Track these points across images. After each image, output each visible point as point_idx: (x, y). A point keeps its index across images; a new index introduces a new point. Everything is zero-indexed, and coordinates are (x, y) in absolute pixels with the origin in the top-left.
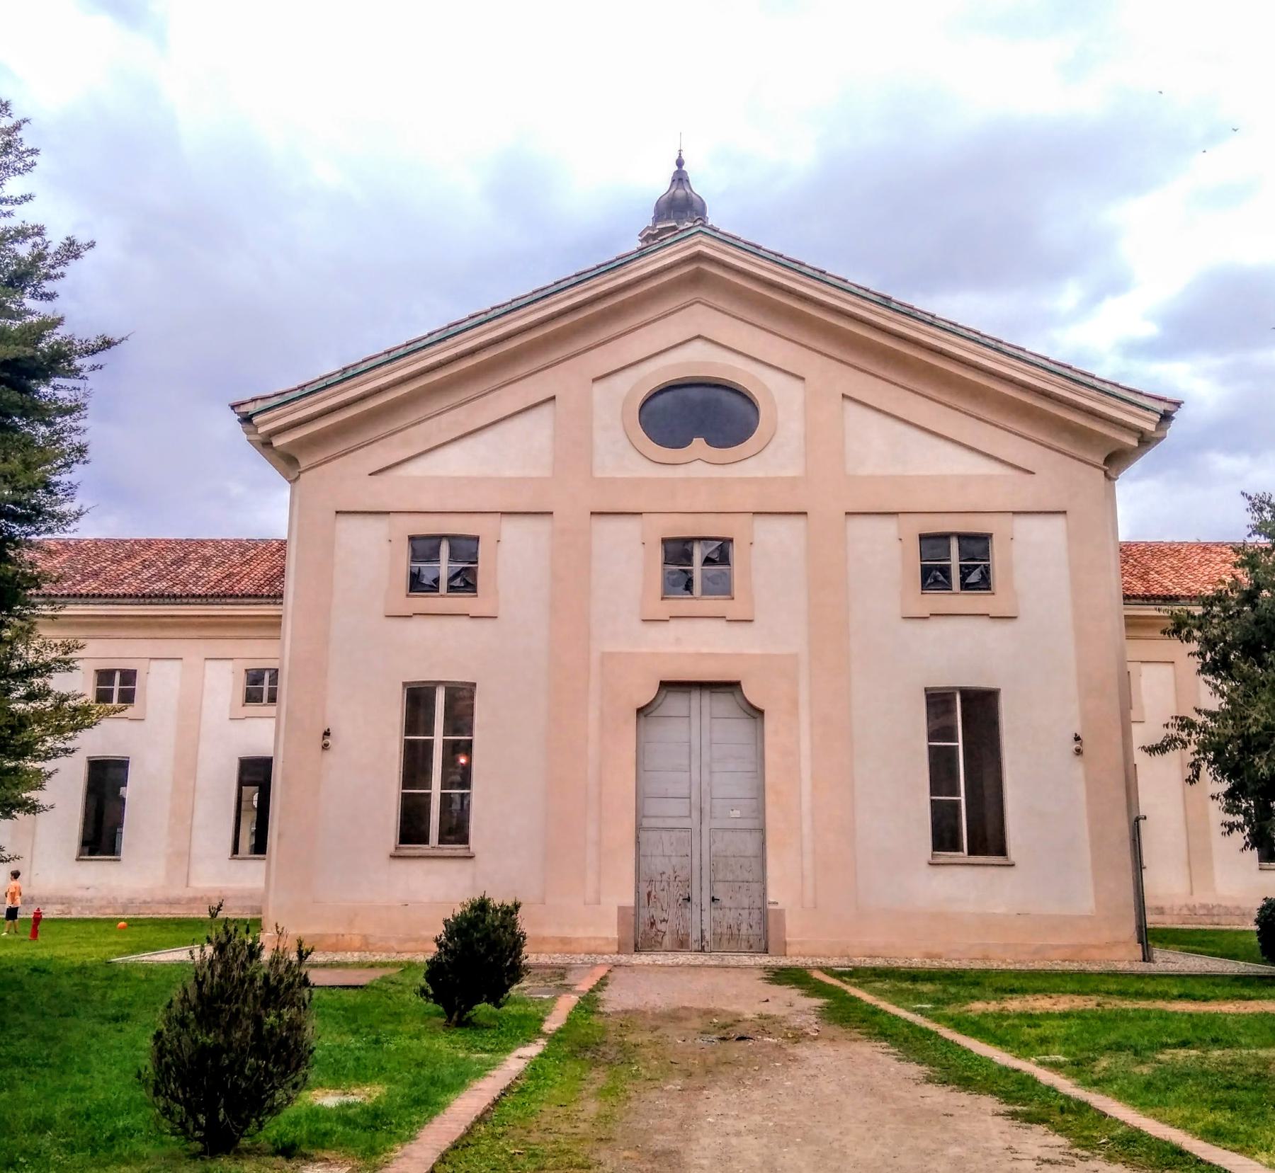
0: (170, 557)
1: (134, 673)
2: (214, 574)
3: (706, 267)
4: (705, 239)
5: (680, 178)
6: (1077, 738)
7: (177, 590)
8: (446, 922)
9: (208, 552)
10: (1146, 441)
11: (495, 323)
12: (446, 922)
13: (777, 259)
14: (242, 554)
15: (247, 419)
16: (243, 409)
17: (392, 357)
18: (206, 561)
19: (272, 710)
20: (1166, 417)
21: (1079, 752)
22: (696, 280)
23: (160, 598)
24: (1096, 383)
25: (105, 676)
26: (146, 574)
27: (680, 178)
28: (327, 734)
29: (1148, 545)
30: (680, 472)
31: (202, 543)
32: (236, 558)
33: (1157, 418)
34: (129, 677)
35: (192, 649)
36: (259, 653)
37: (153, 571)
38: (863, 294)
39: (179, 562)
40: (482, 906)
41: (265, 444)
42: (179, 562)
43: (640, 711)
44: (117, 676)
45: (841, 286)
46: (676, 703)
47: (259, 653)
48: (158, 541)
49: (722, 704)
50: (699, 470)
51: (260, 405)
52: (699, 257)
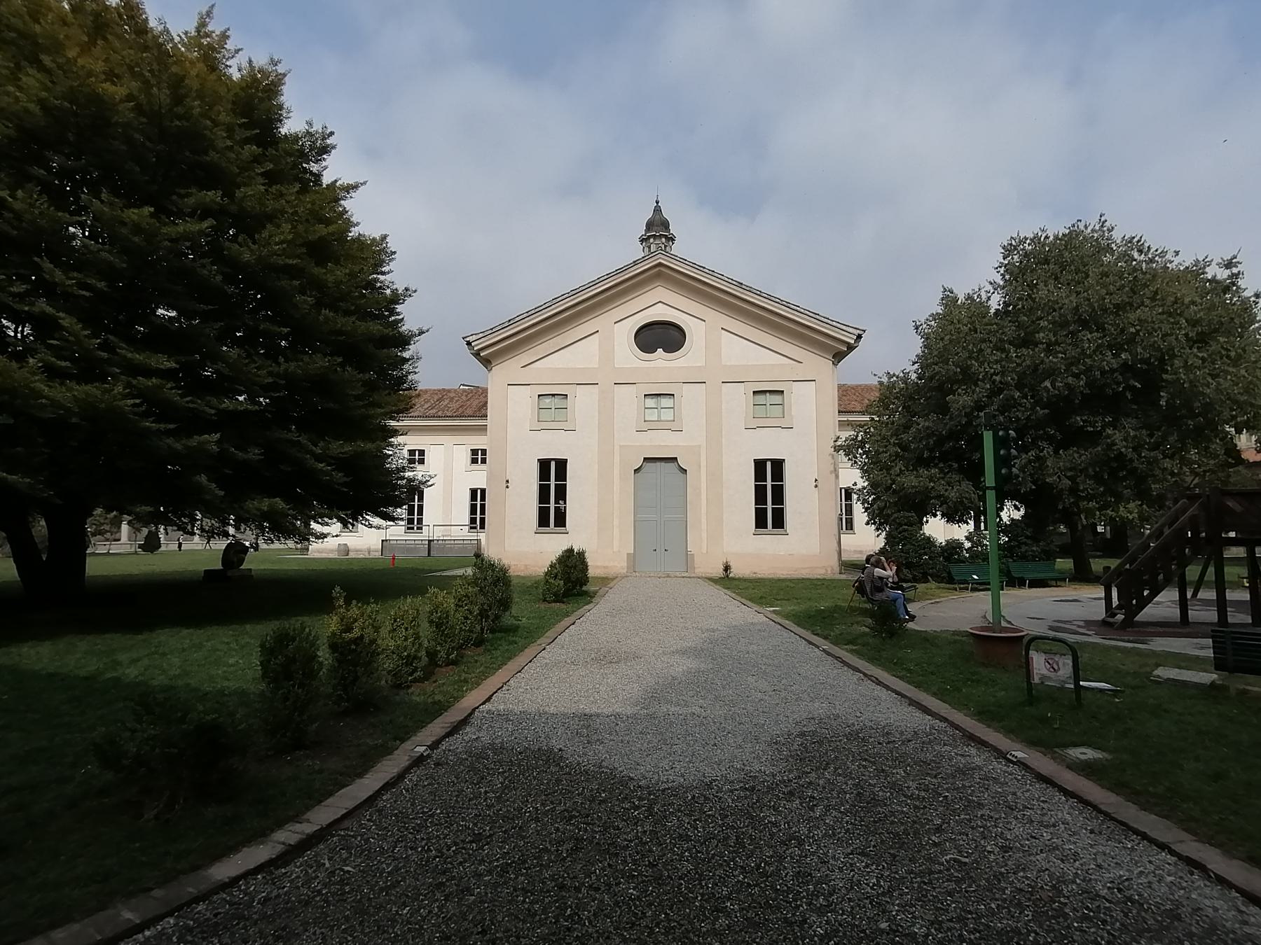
0: (436, 398)
1: (424, 451)
2: (454, 405)
3: (662, 269)
4: (663, 257)
5: (657, 210)
6: (816, 480)
7: (440, 414)
8: (949, 300)
9: (452, 395)
10: (851, 348)
11: (572, 298)
12: (949, 300)
13: (693, 265)
14: (466, 396)
15: (469, 343)
16: (468, 339)
17: (529, 314)
18: (452, 399)
19: (483, 467)
20: (859, 337)
21: (816, 486)
22: (659, 276)
23: (433, 417)
24: (829, 322)
25: (412, 452)
26: (426, 406)
27: (657, 210)
28: (508, 481)
29: (866, 385)
30: (652, 364)
31: (449, 391)
32: (464, 398)
33: (855, 337)
34: (422, 452)
35: (448, 439)
36: (478, 442)
37: (429, 404)
38: (730, 281)
39: (440, 400)
40: (570, 551)
41: (477, 354)
42: (440, 400)
43: (635, 471)
44: (417, 452)
45: (720, 277)
46: (649, 465)
47: (478, 442)
48: (430, 390)
49: (671, 465)
50: (660, 363)
51: (474, 337)
52: (660, 264)
